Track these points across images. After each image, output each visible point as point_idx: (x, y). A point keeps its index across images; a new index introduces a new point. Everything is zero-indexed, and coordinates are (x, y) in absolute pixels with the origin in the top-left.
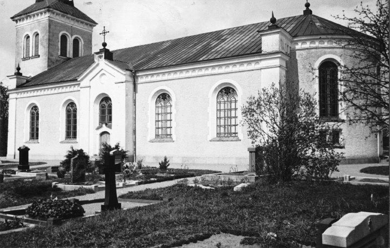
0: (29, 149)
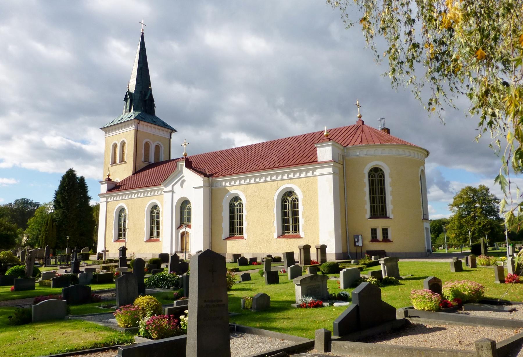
0: (127, 249)
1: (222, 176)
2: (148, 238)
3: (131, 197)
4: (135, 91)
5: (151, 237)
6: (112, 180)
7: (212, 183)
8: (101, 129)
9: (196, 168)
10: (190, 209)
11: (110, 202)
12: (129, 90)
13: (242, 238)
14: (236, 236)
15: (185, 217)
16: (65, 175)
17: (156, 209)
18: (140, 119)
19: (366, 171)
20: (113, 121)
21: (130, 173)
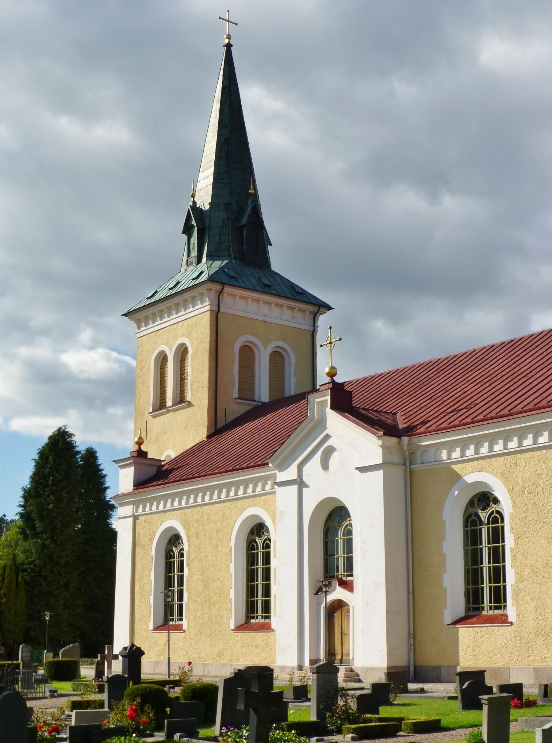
1: (439, 430)
2: (243, 620)
3: (180, 504)
4: (211, 204)
5: (248, 618)
6: (149, 456)
7: (412, 454)
8: (124, 315)
9: (363, 409)
10: (350, 533)
11: (144, 517)
12: (194, 202)
13: (503, 620)
14: (484, 613)
15: (338, 558)
16: (46, 444)
17: (260, 537)
18: (225, 280)
19: (237, 347)
20: (156, 292)
21: (201, 434)
